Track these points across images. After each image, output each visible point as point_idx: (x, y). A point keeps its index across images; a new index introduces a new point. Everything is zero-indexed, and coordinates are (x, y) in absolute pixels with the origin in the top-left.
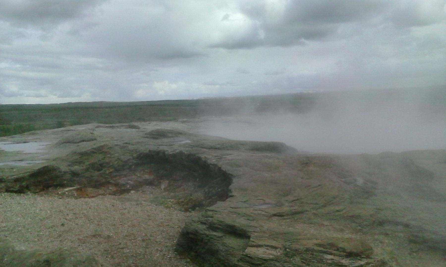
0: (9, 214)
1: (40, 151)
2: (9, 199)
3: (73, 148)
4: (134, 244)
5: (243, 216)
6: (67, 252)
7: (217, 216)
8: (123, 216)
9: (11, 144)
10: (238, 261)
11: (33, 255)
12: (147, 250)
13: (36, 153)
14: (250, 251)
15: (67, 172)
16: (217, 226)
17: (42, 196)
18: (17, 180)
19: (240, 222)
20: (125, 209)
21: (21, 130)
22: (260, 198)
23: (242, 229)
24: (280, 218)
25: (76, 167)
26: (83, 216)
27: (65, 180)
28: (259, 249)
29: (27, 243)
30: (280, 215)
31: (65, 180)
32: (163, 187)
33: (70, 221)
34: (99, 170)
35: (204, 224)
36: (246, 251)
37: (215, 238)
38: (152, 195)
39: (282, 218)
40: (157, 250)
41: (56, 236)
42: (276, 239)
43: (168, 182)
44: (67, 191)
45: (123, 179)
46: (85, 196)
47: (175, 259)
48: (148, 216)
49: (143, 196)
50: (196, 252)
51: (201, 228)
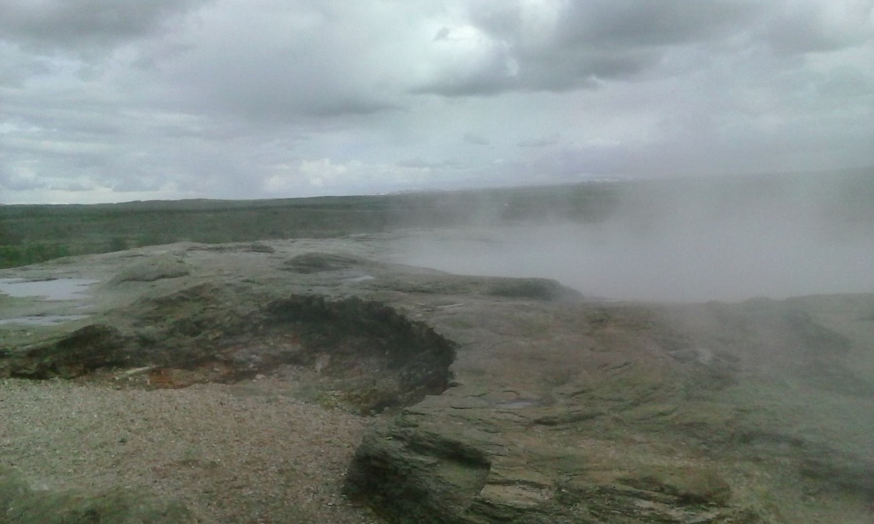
0: (17, 420)
1: (78, 297)
2: (18, 391)
3: (142, 290)
4: (263, 479)
5: (476, 424)
6: (131, 494)
7: (424, 423)
8: (240, 424)
9: (22, 282)
10: (467, 512)
11: (64, 500)
12: (289, 491)
13: (71, 301)
14: (490, 492)
15: (132, 338)
16: (424, 443)
17: (82, 384)
18: (33, 354)
19: (470, 436)
20: (246, 410)
21: (41, 256)
22: (509, 388)
23: (475, 450)
24: (548, 427)
25: (149, 327)
26: (162, 424)
27: (127, 353)
28: (508, 488)
29: (52, 477)
30: (549, 423)
31: (127, 353)
32: (319, 366)
33: (138, 434)
34: (194, 334)
35: (401, 439)
36: (482, 492)
37: (421, 466)
38: (297, 383)
39: (553, 427)
40: (308, 490)
41: (110, 463)
42: (540, 469)
43: (329, 357)
44: (131, 375)
45: (241, 351)
46: (167, 384)
47: (343, 508)
48: (291, 423)
49: (281, 384)
50: (384, 495)
51: (395, 447)
